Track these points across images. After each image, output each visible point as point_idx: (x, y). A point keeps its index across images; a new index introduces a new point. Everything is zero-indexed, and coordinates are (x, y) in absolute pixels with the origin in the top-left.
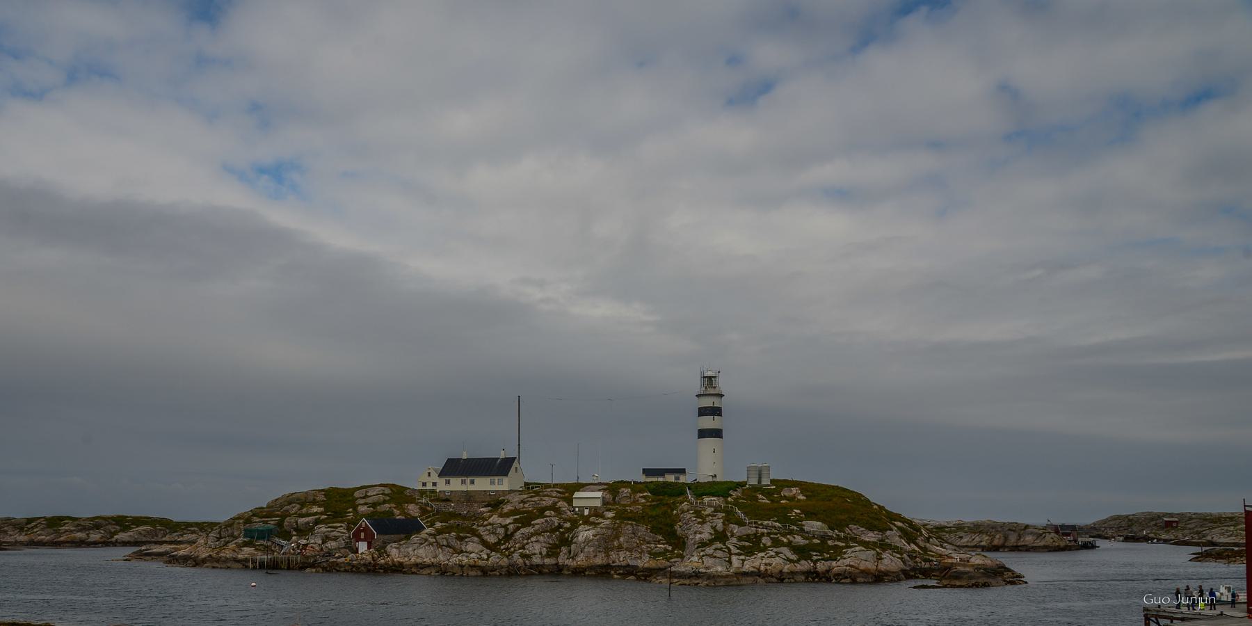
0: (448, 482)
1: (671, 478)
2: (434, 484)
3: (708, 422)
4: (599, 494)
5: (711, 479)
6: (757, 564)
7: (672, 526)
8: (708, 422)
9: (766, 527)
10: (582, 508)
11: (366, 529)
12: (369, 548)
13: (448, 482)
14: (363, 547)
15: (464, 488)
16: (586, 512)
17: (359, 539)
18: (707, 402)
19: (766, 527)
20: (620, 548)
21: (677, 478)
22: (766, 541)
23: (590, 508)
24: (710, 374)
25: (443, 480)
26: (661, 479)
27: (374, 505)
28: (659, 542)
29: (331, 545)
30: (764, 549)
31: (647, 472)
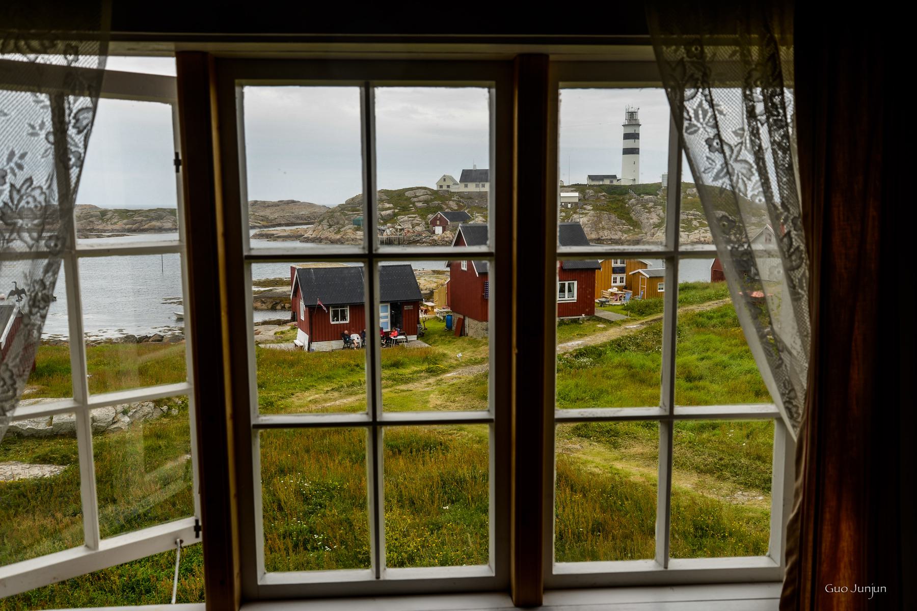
0: (466, 186)
1: (607, 182)
2: (448, 186)
3: (630, 144)
4: (577, 194)
5: (631, 183)
6: (698, 236)
7: (629, 214)
8: (630, 144)
9: (693, 215)
10: (566, 204)
11: (441, 219)
12: (444, 230)
13: (466, 186)
14: (439, 230)
15: (477, 190)
16: (569, 206)
17: (435, 225)
18: (630, 130)
19: (693, 215)
20: (603, 228)
21: (612, 182)
22: (695, 223)
23: (572, 203)
24: (632, 110)
25: (463, 185)
26: (601, 183)
27: (425, 202)
28: (624, 224)
29: (418, 229)
30: (696, 228)
31: (591, 178)
